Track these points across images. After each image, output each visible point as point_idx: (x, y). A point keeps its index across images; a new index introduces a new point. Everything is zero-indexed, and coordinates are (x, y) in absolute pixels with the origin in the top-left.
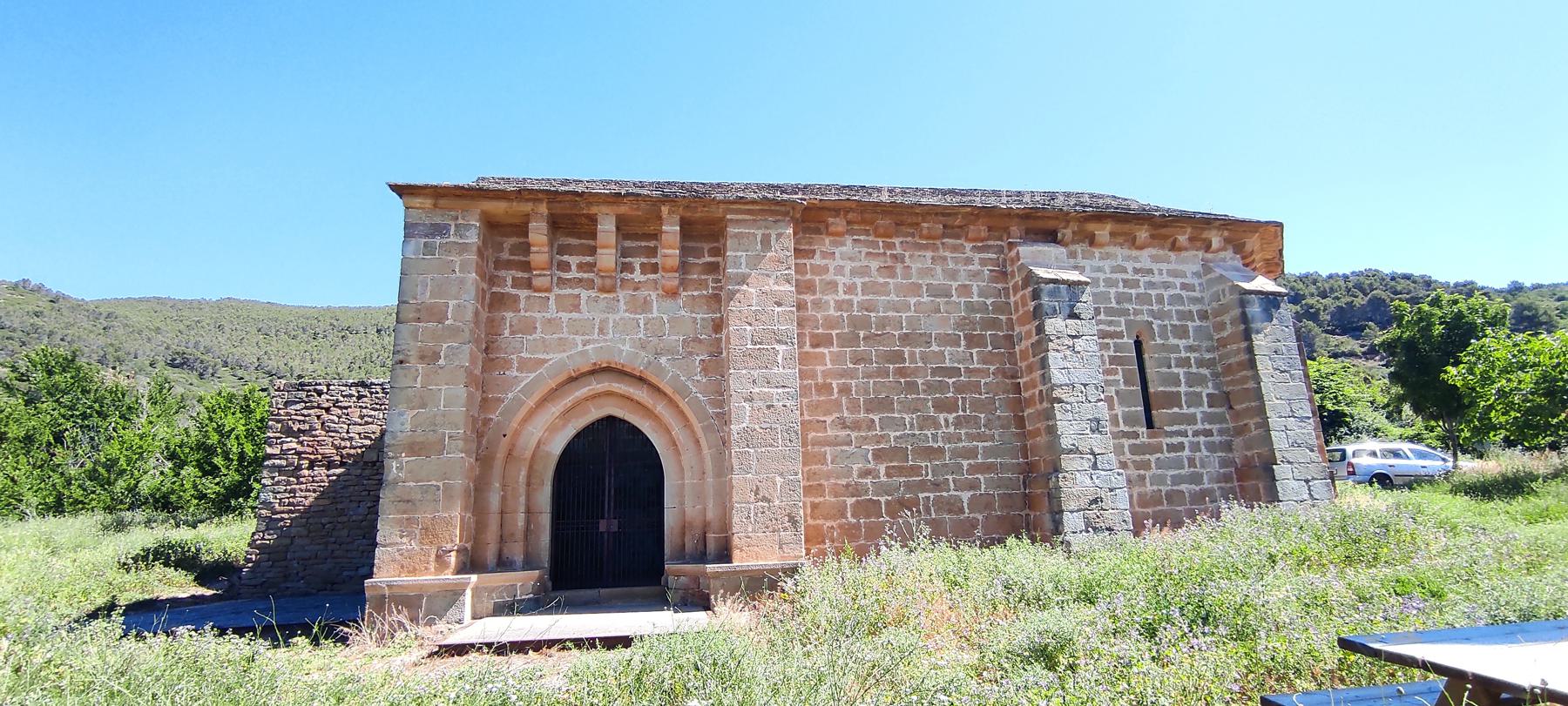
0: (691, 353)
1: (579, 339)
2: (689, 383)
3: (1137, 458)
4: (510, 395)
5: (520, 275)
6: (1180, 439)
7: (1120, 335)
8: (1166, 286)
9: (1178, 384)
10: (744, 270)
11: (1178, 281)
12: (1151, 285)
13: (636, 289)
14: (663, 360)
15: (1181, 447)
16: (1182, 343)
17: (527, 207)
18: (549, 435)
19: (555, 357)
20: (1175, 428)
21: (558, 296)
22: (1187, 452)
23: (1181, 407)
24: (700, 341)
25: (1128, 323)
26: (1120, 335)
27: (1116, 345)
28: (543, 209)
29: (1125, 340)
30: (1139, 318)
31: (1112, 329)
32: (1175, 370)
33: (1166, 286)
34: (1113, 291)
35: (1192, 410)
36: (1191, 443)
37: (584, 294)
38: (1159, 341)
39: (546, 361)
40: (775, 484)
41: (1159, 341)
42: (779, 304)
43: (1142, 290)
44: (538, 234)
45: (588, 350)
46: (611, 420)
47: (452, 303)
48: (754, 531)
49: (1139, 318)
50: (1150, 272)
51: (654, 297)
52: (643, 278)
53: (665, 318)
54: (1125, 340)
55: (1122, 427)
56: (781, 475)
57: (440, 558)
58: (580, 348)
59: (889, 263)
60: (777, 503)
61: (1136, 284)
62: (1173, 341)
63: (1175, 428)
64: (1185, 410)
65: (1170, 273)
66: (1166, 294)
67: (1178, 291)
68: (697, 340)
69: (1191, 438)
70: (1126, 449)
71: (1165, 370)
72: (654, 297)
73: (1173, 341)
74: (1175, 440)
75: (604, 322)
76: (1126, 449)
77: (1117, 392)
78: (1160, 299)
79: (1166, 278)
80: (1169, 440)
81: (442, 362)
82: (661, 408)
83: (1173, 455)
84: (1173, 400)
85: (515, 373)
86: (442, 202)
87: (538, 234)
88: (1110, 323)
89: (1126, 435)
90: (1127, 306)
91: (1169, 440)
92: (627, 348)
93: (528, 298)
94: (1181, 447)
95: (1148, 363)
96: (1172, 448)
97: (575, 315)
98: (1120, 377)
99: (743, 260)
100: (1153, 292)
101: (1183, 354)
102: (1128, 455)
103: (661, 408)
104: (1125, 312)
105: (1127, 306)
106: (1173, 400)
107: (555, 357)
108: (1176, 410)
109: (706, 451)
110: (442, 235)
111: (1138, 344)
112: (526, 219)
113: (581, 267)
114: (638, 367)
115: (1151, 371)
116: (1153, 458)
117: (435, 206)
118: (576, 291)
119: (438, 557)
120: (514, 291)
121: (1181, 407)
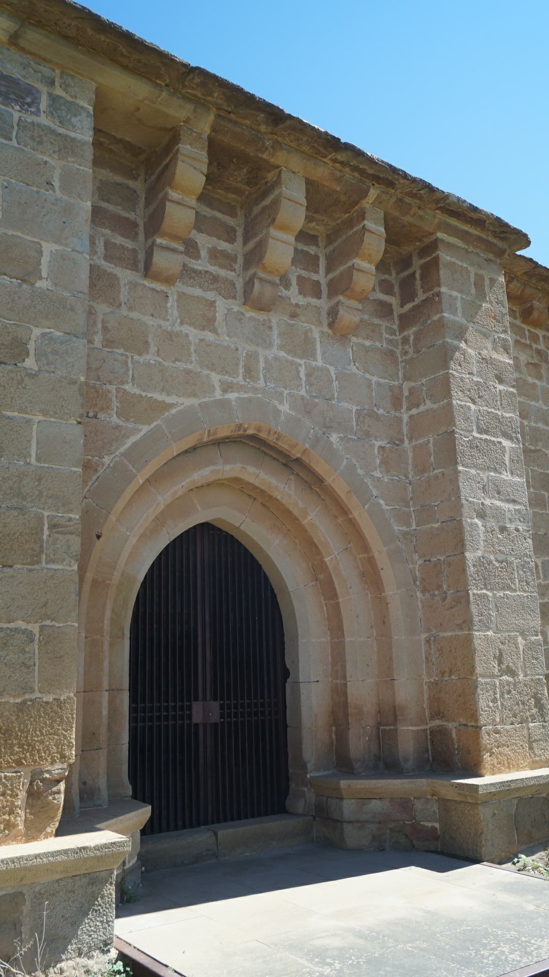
0: (367, 434)
1: (215, 378)
2: (368, 481)
4: (107, 460)
5: (119, 240)
10: (459, 319)
13: (294, 316)
14: (334, 438)
17: (178, 111)
18: (135, 548)
19: (182, 402)
21: (182, 296)
24: (378, 418)
28: (205, 125)
37: (222, 305)
39: (167, 407)
40: (516, 645)
42: (501, 381)
44: (190, 170)
45: (228, 398)
46: (205, 528)
47: (49, 248)
48: (502, 722)
51: (316, 334)
52: (301, 300)
53: (332, 370)
56: (522, 634)
57: (36, 796)
58: (218, 395)
59: (535, 361)
60: (521, 677)
68: (372, 415)
72: (316, 334)
75: (252, 357)
81: (30, 363)
82: (315, 518)
85: (115, 420)
86: (33, 37)
87: (190, 170)
92: (285, 408)
93: (133, 285)
97: (209, 336)
99: (459, 304)
103: (315, 518)
107: (182, 402)
109: (392, 591)
110: (25, 106)
112: (173, 137)
113: (214, 255)
114: (299, 438)
117: (14, 39)
118: (210, 295)
119: (33, 795)
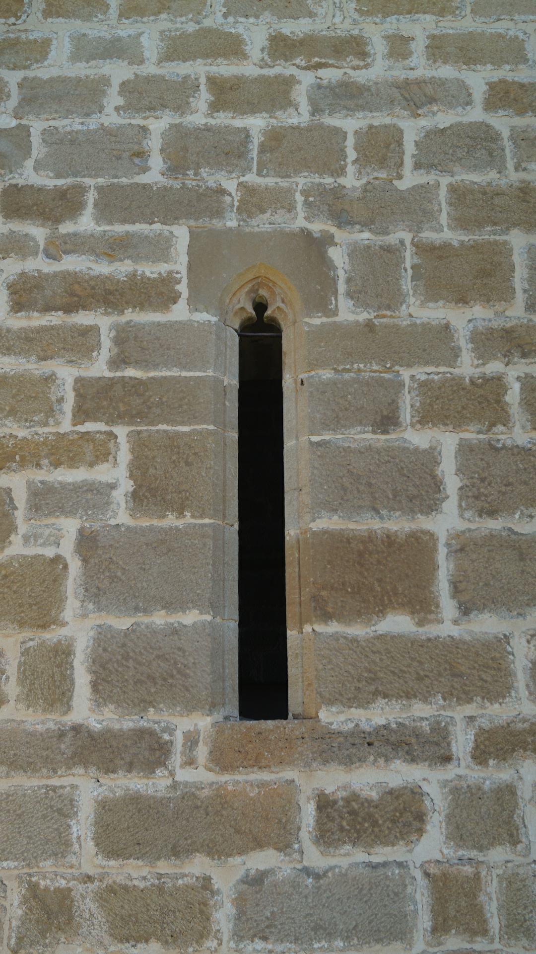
3: (135, 872)
6: (400, 773)
7: (160, 293)
8: (415, 96)
9: (424, 493)
11: (478, 80)
12: (348, 96)
15: (402, 814)
16: (463, 319)
20: (379, 715)
22: (432, 845)
23: (422, 605)
25: (203, 252)
26: (160, 293)
27: (123, 336)
29: (180, 312)
30: (262, 223)
31: (122, 269)
32: (418, 438)
33: (415, 96)
34: (159, 125)
35: (487, 624)
36: (464, 798)
38: (347, 312)
41: (347, 312)
43: (299, 116)
49: (262, 223)
50: (353, 47)
54: (180, 312)
55: (84, 710)
61: (276, 94)
62: (419, 311)
63: (379, 715)
64: (448, 624)
65: (438, 48)
66: (411, 130)
67: (476, 114)
69: (464, 769)
70: (82, 827)
71: (362, 436)
73: (419, 311)
74: (370, 779)
76: (82, 827)
77: (87, 543)
78: (381, 148)
79: (419, 66)
80: (334, 780)
83: (349, 857)
84: (390, 573)
88: (115, 248)
89: (94, 750)
90: (212, 178)
91: (334, 780)
94: (402, 814)
95: (297, 586)
96: (346, 820)
98: (117, 474)
100: (351, 124)
101: (467, 366)
102: (87, 857)
104: (209, 202)
105: (212, 178)
106: (390, 573)
108: (398, 623)
111: (260, 352)
115: (305, 520)
116: (226, 876)
120: (494, 367)
121: (422, 605)
